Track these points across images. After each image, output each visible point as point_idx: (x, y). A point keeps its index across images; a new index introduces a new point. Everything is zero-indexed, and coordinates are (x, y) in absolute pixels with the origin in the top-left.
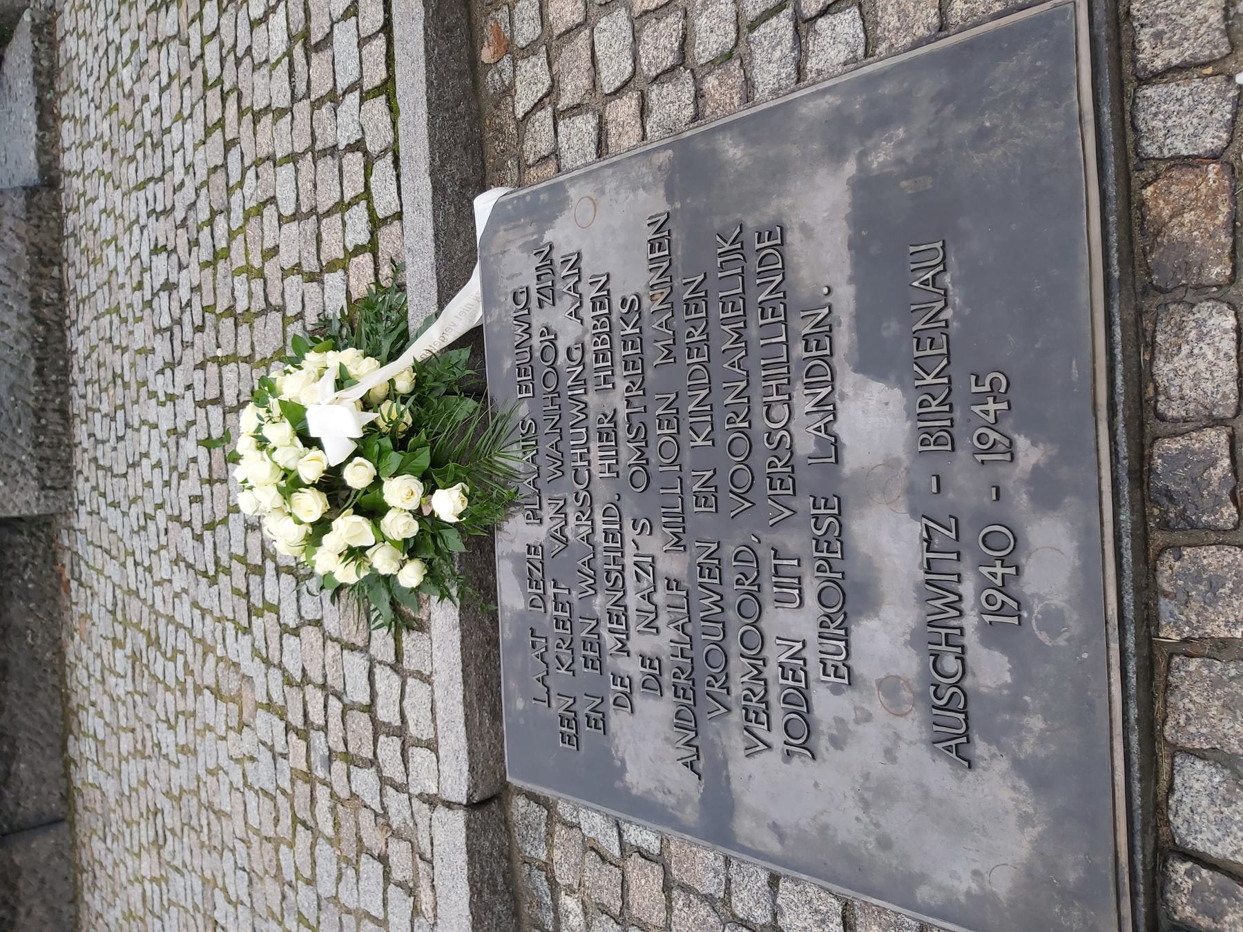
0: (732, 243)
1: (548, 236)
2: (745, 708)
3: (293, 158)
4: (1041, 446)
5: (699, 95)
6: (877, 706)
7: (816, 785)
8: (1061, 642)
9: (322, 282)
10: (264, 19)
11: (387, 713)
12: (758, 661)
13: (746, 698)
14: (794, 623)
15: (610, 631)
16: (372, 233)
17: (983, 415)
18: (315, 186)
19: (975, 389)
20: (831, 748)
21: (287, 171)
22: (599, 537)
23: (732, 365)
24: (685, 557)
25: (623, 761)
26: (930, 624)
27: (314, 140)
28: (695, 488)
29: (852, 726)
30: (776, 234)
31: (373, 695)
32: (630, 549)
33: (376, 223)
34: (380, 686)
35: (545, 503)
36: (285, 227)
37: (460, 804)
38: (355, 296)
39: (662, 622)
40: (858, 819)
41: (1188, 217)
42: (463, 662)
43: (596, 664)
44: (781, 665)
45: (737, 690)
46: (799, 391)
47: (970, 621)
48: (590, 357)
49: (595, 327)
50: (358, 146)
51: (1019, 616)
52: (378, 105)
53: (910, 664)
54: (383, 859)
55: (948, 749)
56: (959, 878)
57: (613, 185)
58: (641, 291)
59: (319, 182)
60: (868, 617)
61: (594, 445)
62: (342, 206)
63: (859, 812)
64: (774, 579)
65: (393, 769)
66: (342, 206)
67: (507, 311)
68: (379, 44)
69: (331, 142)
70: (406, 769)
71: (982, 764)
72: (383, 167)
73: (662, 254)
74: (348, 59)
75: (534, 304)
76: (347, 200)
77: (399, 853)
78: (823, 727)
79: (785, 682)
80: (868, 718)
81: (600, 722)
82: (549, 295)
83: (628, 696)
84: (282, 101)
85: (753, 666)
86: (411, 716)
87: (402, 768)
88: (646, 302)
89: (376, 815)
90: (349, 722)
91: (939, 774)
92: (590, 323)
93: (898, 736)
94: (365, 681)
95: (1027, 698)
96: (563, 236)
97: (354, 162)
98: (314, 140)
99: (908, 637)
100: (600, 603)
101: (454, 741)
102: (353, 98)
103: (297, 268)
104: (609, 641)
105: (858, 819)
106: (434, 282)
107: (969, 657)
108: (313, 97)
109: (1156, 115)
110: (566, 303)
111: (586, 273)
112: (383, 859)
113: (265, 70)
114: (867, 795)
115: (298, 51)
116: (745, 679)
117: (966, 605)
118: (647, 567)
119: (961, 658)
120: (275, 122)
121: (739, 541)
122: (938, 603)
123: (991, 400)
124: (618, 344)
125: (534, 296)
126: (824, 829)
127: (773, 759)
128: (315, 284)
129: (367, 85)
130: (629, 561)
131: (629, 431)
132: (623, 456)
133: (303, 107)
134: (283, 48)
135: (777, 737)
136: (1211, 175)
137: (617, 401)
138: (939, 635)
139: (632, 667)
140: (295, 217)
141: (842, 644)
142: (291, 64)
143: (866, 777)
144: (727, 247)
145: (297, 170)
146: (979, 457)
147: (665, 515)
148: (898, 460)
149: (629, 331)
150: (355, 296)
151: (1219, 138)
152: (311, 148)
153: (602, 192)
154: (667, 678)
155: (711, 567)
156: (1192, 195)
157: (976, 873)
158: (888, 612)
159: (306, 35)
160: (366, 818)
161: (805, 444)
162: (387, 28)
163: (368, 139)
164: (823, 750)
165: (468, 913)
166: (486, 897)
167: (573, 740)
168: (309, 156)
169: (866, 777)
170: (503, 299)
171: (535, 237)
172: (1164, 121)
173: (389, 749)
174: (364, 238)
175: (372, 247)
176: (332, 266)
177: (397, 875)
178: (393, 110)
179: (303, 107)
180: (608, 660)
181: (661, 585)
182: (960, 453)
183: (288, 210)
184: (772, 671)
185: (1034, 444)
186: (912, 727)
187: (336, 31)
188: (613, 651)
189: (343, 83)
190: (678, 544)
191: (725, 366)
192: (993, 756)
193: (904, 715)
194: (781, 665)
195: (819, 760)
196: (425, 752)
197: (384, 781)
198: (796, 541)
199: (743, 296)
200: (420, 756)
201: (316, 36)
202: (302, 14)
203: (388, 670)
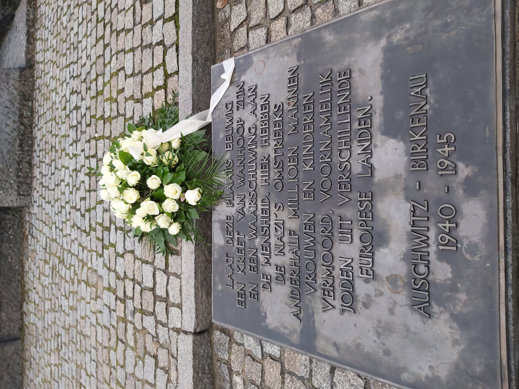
2: (324, 289)
4: (470, 167)
6: (386, 288)
7: (355, 325)
11: (160, 292)
12: (330, 268)
13: (324, 285)
14: (348, 250)
15: (263, 254)
19: (439, 141)
20: (363, 308)
22: (259, 212)
25: (266, 313)
26: (413, 250)
29: (373, 298)
32: (273, 217)
33: (167, 76)
34: (158, 280)
37: (191, 332)
38: (156, 108)
40: (375, 341)
42: (195, 269)
44: (341, 269)
50: (161, 43)
53: (402, 269)
54: (155, 357)
55: (420, 309)
56: (422, 370)
57: (273, 54)
61: (259, 171)
63: (375, 338)
66: (153, 69)
70: (168, 316)
71: (436, 316)
73: (294, 84)
77: (162, 354)
78: (360, 298)
80: (381, 294)
81: (255, 295)
82: (241, 104)
86: (171, 293)
87: (166, 316)
89: (153, 337)
91: (414, 320)
92: (259, 116)
93: (395, 303)
99: (402, 257)
102: (160, 22)
103: (132, 97)
105: (375, 341)
107: (431, 266)
108: (143, 23)
110: (249, 108)
112: (155, 357)
113: (123, 13)
114: (380, 330)
117: (431, 241)
119: (427, 266)
120: (126, 35)
122: (417, 240)
123: (446, 146)
124: (272, 125)
126: (358, 346)
127: (335, 313)
130: (272, 223)
132: (272, 173)
135: (337, 303)
138: (417, 256)
139: (271, 271)
142: (134, 10)
143: (380, 322)
144: (324, 80)
145: (134, 55)
147: (290, 201)
149: (277, 119)
152: (141, 45)
154: (287, 276)
155: (310, 225)
157: (431, 367)
158: (393, 245)
160: (149, 338)
166: (200, 375)
169: (380, 322)
173: (160, 307)
175: (165, 87)
176: (147, 96)
177: (161, 364)
179: (138, 28)
181: (287, 233)
184: (337, 272)
185: (467, 166)
188: (263, 263)
190: (296, 215)
192: (441, 312)
193: (399, 293)
194: (341, 269)
195: (357, 313)
196: (176, 309)
197: (157, 322)
198: (350, 213)
200: (174, 311)
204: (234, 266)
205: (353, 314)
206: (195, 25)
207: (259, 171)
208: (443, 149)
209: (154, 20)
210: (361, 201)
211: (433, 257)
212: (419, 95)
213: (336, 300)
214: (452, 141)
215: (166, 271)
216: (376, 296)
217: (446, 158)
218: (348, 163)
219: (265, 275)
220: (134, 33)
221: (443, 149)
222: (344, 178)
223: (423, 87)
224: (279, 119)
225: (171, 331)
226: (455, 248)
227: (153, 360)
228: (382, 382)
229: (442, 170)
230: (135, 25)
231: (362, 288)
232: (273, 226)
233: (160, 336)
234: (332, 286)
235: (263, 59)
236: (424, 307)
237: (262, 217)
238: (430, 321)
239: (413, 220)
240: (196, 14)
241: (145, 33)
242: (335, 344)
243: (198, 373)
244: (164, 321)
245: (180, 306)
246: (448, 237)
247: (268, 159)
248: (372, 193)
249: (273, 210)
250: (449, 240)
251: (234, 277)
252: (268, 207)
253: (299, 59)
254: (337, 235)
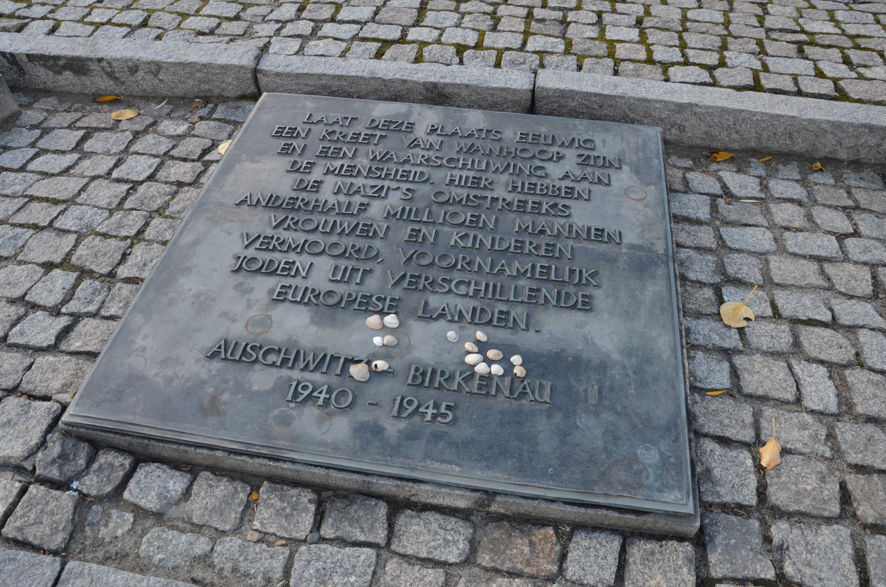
0: (587, 279)
1: (625, 168)
2: (272, 238)
3: (727, 24)
4: (397, 435)
5: (702, 284)
6: (254, 312)
7: (216, 270)
8: (270, 421)
9: (635, 26)
10: (832, 19)
11: (328, 29)
12: (301, 249)
13: (278, 239)
14: (321, 273)
15: (342, 166)
16: (660, 62)
17: (426, 405)
18: (703, 33)
20: (235, 283)
21: (719, 18)
22: (407, 167)
23: (503, 266)
24: (379, 218)
25: (258, 161)
26: (298, 353)
27: (736, 37)
28: (544, 290)
29: (247, 296)
30: (587, 306)
31: (342, 22)
32: (394, 185)
33: (665, 66)
34: (346, 27)
35: (440, 139)
36: (680, 11)
37: (258, 64)
38: (618, 46)
39: (342, 198)
40: (190, 290)
41: (526, 550)
42: (348, 76)
43: (324, 154)
44: (294, 263)
45: (284, 235)
46: (471, 303)
47: (296, 374)
48: (534, 180)
49: (554, 186)
50: (722, 64)
51: (291, 402)
52: (749, 80)
53: (276, 336)
54: (237, 18)
55: (220, 347)
56: (143, 339)
57: (649, 213)
58: (571, 220)
59: (704, 36)
60: (312, 318)
61: (471, 174)
62: (683, 46)
63: (194, 291)
64: (350, 267)
65: (289, 29)
66: (683, 46)
67: (581, 135)
68: (790, 86)
69: (730, 47)
70: (289, 37)
71: (207, 364)
72: (705, 76)
73: (593, 235)
74: (785, 65)
75: (581, 152)
76: (687, 50)
77: (237, 28)
78: (250, 280)
79: (283, 262)
80: (249, 306)
81: (286, 151)
82: (585, 161)
83: (298, 170)
84: (769, 22)
85: (297, 247)
86: (321, 43)
87: (291, 33)
88: (562, 221)
89: (264, 17)
90: (328, 6)
91: (208, 340)
92: (558, 184)
93: (234, 321)
94: (351, 18)
95: (240, 396)
96: (623, 178)
97: (712, 59)
98: (736, 37)
99: (294, 338)
100: (363, 162)
101: (298, 65)
102: (757, 65)
103: (648, 13)
104: (338, 164)
105: (190, 290)
106: (614, 93)
107: (274, 370)
108: (766, 41)
109: (601, 544)
110: (578, 172)
111: (595, 188)
112: (237, 18)
113: (795, 14)
114: (202, 298)
115: (803, 37)
116: (291, 240)
117: (307, 375)
118: (379, 193)
119: (274, 364)
120: (757, 16)
121: (382, 251)
122: (311, 358)
123: (435, 412)
124: (537, 199)
125: (586, 153)
126: (189, 270)
127: (238, 248)
128: (634, 23)
129: (762, 75)
130: (386, 183)
131: (475, 196)
132: (460, 191)
133: (761, 34)
134: (807, 28)
135: (251, 253)
136: (549, 567)
137: (500, 192)
138: (290, 356)
139: (317, 174)
140: (685, 19)
141: (298, 299)
142: (795, 32)
143: (214, 299)
144: (585, 275)
145: (717, 24)
146: (399, 399)
147: (411, 210)
148: (410, 352)
150: (618, 46)
151: (574, 575)
152: (730, 34)
153: (646, 206)
154: (304, 195)
155: (367, 232)
156: (541, 555)
157: (144, 349)
158: (313, 329)
159: (812, 43)
160: (263, 10)
161: (436, 301)
162: (799, 93)
163: (725, 69)
164: (236, 277)
165: (190, 61)
166: (198, 75)
167: (279, 134)
168: (725, 32)
169: (214, 299)
170: (590, 133)
171: (628, 161)
172: (594, 547)
173: (305, 27)
174: (657, 56)
175: (650, 61)
176: (642, 34)
177: (225, 25)
178: (739, 88)
179: (761, 34)
180: (323, 162)
181: (365, 200)
182: (405, 388)
183: (690, 15)
184: (292, 257)
185: (399, 431)
186: (238, 331)
187: (808, 62)
188: (329, 164)
189: (769, 61)
190: (389, 216)
191: (503, 261)
192: (210, 371)
193: (246, 327)
194: (294, 263)
195: (231, 274)
196: (297, 48)
197: (285, 23)
198: (372, 285)
199: (548, 280)
200: (295, 44)
201: (808, 50)
202: (827, 43)
203: (355, 33)
204: (337, 128)
205: (230, 269)
207: (471, 174)
209: (765, 58)
210: (385, 299)
211: (285, 372)
213: (255, 252)
215: (355, 38)
216: (248, 300)
218: (447, 289)
219: (311, 165)
220: (755, 27)
222: (426, 283)
225: (268, 39)
226: (289, 398)
227: (232, 15)
230: (768, 30)
231: (264, 285)
232: (380, 183)
233: (265, 25)
234: (274, 249)
235: (648, 198)
237: (397, 171)
238: (201, 356)
240: (754, 118)
241: (749, 42)
242: (197, 243)
243: (200, 71)
244: (285, 32)
245: (300, 51)
247: (485, 188)
249: (404, 186)
251: (321, 126)
252: (411, 179)
253: (632, 247)
254: (343, 263)
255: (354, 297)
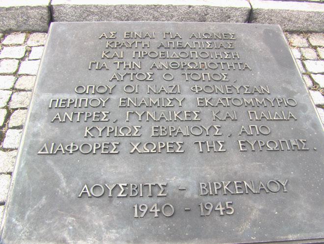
19: (227, 203)
149: (207, 101)
206: (293, 60)
208: (221, 206)
212: (216, 188)
214: (227, 213)
217: (213, 209)
221: (221, 206)
223: (267, 190)
224: (206, 103)
228: (16, 162)
229: (138, 208)
236: (87, 193)
239: (148, 185)
246: (145, 211)
248: (225, 152)
250: (208, 210)
255: (100, 146)
